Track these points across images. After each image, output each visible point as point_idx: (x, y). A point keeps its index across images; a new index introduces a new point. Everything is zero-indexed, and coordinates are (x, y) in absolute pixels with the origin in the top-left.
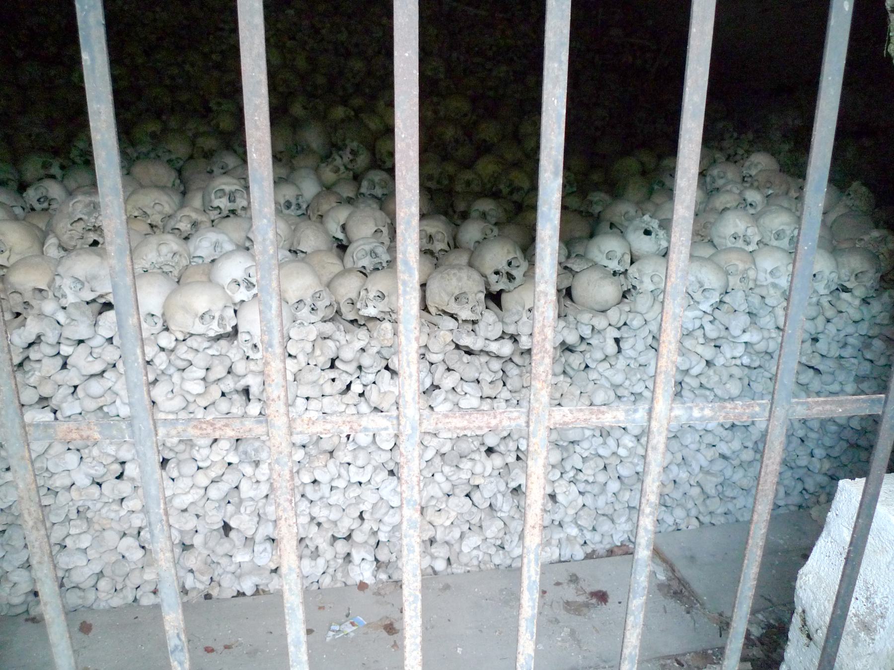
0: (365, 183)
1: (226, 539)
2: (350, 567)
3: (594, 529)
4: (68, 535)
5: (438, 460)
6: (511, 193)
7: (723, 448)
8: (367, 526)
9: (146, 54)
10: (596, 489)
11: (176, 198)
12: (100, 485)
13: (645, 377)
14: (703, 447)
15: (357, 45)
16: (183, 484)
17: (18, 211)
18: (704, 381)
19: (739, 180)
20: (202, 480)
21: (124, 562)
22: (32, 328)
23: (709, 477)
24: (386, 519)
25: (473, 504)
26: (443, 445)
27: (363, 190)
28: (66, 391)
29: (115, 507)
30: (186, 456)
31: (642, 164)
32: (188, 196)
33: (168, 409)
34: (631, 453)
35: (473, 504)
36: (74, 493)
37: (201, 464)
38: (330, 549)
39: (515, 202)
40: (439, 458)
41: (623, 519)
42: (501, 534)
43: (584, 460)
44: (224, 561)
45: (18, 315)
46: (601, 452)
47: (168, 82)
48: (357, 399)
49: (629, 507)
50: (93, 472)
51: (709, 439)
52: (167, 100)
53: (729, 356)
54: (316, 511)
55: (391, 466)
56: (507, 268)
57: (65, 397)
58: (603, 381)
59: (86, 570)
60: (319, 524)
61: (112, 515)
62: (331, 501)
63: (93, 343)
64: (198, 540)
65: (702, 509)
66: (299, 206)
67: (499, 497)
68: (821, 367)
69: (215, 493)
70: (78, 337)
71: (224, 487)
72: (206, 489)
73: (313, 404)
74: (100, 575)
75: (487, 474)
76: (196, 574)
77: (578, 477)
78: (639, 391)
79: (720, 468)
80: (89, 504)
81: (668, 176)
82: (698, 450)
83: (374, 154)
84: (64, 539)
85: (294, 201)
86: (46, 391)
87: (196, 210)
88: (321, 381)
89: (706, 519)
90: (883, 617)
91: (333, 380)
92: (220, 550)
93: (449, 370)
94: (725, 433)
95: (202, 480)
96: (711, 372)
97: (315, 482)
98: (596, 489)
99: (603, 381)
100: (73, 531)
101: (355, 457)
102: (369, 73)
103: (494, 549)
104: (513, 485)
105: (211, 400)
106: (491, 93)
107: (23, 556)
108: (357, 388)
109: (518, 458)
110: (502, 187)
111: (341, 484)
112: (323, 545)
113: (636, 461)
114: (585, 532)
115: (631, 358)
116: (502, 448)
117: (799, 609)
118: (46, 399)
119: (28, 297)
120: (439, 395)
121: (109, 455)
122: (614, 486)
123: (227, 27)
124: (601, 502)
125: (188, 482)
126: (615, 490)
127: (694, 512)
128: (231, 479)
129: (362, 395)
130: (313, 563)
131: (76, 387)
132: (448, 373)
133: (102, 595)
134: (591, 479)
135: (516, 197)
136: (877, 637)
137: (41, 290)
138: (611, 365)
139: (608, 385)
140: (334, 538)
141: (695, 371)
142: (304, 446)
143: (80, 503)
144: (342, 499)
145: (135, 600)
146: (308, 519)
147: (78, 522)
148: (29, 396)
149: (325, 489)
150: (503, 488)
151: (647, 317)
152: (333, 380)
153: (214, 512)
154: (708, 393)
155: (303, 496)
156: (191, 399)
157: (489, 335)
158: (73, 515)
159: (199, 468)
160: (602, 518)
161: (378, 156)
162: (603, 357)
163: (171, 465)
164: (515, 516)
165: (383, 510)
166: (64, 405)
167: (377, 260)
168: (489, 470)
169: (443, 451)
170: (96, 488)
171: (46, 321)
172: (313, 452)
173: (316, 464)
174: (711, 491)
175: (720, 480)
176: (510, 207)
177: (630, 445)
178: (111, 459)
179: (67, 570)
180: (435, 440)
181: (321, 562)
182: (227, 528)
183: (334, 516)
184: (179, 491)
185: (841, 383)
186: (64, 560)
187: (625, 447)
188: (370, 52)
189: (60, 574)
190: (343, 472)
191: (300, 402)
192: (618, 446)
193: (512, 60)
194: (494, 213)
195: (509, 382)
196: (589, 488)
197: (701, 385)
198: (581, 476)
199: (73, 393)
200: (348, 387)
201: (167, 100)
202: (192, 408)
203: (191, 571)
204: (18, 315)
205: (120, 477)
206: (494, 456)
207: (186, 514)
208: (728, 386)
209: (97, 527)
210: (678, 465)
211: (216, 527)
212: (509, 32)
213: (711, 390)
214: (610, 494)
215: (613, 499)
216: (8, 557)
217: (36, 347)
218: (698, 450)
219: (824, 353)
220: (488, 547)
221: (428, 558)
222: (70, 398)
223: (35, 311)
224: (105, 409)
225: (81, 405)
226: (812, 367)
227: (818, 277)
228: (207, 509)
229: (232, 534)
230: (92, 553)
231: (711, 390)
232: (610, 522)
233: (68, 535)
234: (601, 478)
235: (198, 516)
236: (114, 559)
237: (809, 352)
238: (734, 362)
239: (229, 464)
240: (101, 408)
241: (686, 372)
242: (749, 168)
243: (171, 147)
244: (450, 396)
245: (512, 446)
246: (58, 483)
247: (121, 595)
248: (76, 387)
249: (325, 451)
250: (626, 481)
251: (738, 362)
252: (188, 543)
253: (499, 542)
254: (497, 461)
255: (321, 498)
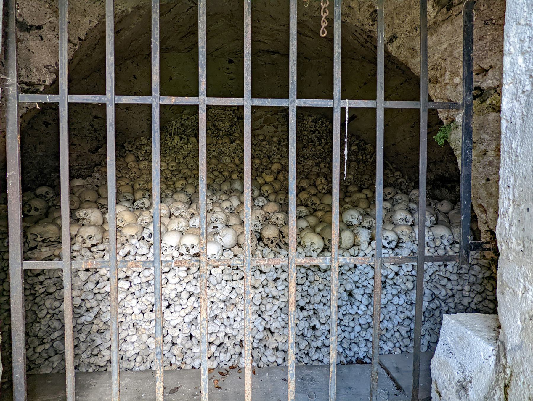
0: (256, 201)
1: (189, 341)
2: (241, 358)
3: (350, 350)
4: (128, 335)
5: (279, 311)
6: (312, 205)
7: (408, 313)
9: (184, 159)
10: (350, 329)
11: (187, 206)
12: (143, 313)
13: (368, 279)
14: (399, 312)
15: (257, 155)
16: (175, 315)
17: (131, 209)
18: (395, 281)
19: (408, 200)
20: (183, 313)
21: (148, 349)
22: (127, 248)
23: (403, 327)
24: (257, 336)
26: (281, 304)
27: (255, 204)
28: (136, 274)
29: (148, 324)
30: (177, 303)
31: (366, 195)
32: (192, 205)
34: (364, 313)
36: (133, 317)
37: (183, 307)
38: (233, 349)
39: (313, 209)
40: (279, 310)
41: (364, 345)
42: (307, 348)
43: (344, 315)
44: (188, 352)
45: (124, 244)
46: (351, 312)
47: (190, 168)
49: (366, 340)
50: (141, 308)
51: (400, 309)
52: (189, 173)
53: (405, 271)
54: (227, 330)
55: (259, 313)
57: (135, 276)
58: (350, 280)
59: (133, 351)
60: (229, 337)
61: (146, 327)
62: (234, 327)
63: (148, 256)
64: (179, 341)
65: (401, 344)
66: (231, 209)
67: (306, 330)
68: (451, 278)
69: (188, 319)
70: (142, 253)
71: (191, 317)
72: (184, 317)
73: (229, 284)
74: (138, 354)
75: (300, 319)
76: (177, 356)
77: (341, 323)
78: (366, 285)
79: (408, 324)
80: (138, 322)
82: (396, 314)
83: (261, 191)
84: (126, 337)
85: (229, 207)
86: (128, 274)
87: (194, 210)
88: (232, 274)
89: (404, 349)
90: (470, 382)
91: (237, 274)
92: (187, 346)
93: (283, 271)
94: (408, 306)
95: (183, 313)
96: (398, 277)
97: (228, 317)
98: (350, 329)
99: (350, 280)
100: (130, 333)
102: (261, 164)
103: (304, 355)
104: (312, 325)
105: (189, 280)
106: (306, 171)
107: (109, 344)
109: (315, 313)
110: (309, 202)
111: (238, 319)
112: (230, 348)
113: (367, 317)
114: (346, 350)
115: (361, 270)
116: (307, 307)
117: (434, 380)
118: (129, 277)
119: (128, 237)
120: (279, 282)
121: (148, 301)
122: (358, 328)
123: (212, 150)
124: (352, 336)
125: (177, 314)
126: (359, 331)
127: (397, 345)
128: (194, 313)
130: (225, 355)
131: (140, 273)
132: (282, 273)
133: (137, 364)
134: (347, 325)
135: (314, 207)
136: (470, 393)
137: (133, 236)
138: (353, 273)
139: (352, 282)
140: (235, 344)
141: (390, 277)
142: (224, 302)
143: (134, 321)
144: (239, 326)
145: (150, 368)
146: (224, 334)
147: (133, 329)
148: (122, 275)
149: (232, 321)
150: (307, 326)
151: (366, 252)
152: (237, 274)
153: (186, 328)
154: (398, 287)
155: (222, 323)
156: (182, 279)
158: (131, 326)
159: (182, 308)
160: (353, 344)
161: (262, 192)
162: (349, 269)
163: (171, 307)
165: (255, 332)
166: (135, 280)
167: (256, 228)
168: (301, 317)
169: (281, 307)
170: (142, 315)
171: (132, 246)
173: (229, 309)
174: (405, 335)
175: (409, 329)
176: (311, 210)
177: (364, 309)
178: (149, 303)
179: (126, 351)
180: (278, 302)
181: (228, 355)
182: (191, 336)
183: (235, 333)
184: (173, 318)
185: (462, 285)
186: (124, 347)
187: (361, 310)
188: (262, 157)
189: (122, 353)
190: (239, 313)
192: (358, 309)
193: (315, 159)
194: (304, 212)
195: (309, 278)
196: (346, 329)
197: (395, 284)
198: (342, 323)
199: (139, 275)
201: (189, 173)
202: (182, 282)
203: (175, 355)
204: (124, 244)
205: (152, 311)
206: (303, 311)
207: (175, 329)
208: (406, 284)
209: (140, 332)
210: (388, 321)
211: (186, 335)
212: (314, 149)
213: (399, 286)
214: (356, 333)
215: (358, 335)
216: (103, 344)
217: (128, 257)
218: (396, 314)
219: (451, 271)
220: (302, 354)
221: (275, 357)
222: (137, 277)
223: (129, 243)
224: (150, 282)
225: (141, 280)
226: (447, 278)
227: (444, 237)
228: (184, 327)
229: (193, 339)
230: (136, 344)
231: (399, 286)
232: (357, 347)
233: (128, 335)
234: (352, 324)
235: (180, 330)
236: (144, 347)
237: (444, 270)
238: (408, 273)
239: (194, 307)
240: (148, 282)
241: (386, 277)
242: (412, 195)
244: (285, 283)
245: (311, 307)
246: (127, 312)
247: (145, 365)
248: (140, 273)
249: (233, 304)
250: (363, 326)
251: (410, 273)
252: (175, 342)
253: (306, 352)
254: (305, 313)
255: (230, 325)
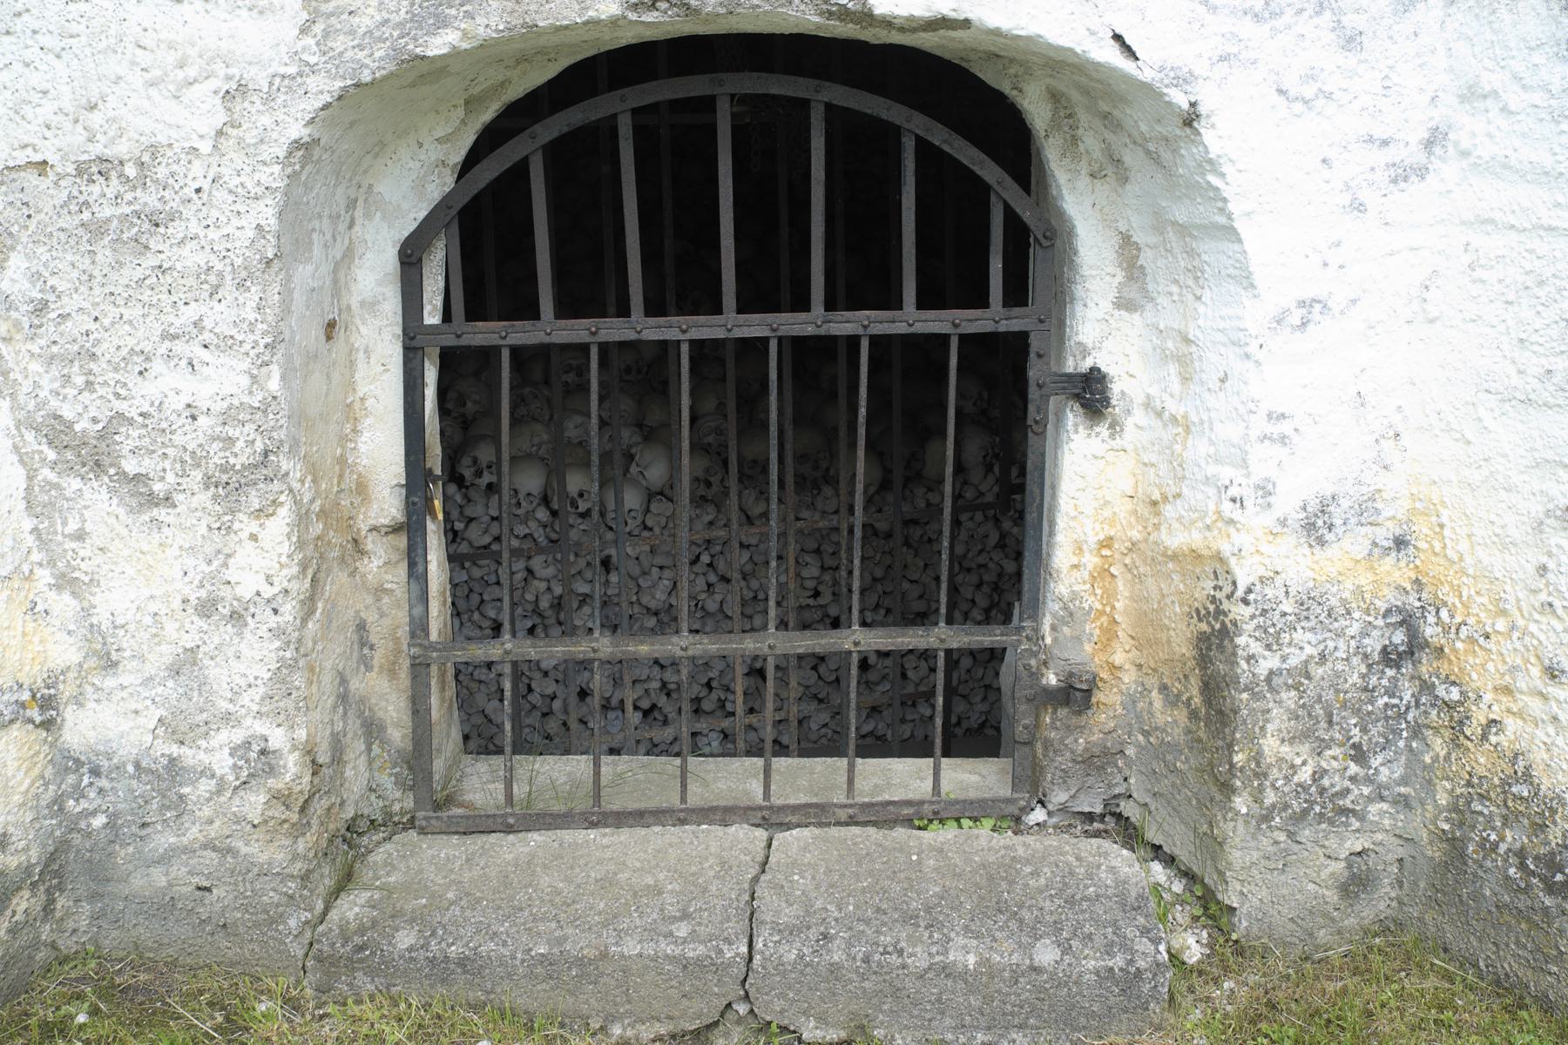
8: (714, 696)
25: (820, 677)
33: (544, 576)
35: (820, 677)
41: (979, 698)
48: (705, 569)
56: (484, 465)
81: (1073, 417)
101: (704, 625)
108: (705, 559)
129: (710, 565)
157: (826, 508)
164: (1011, 524)
172: (666, 619)
191: (655, 571)
200: (698, 557)
214: (963, 672)
243: (1081, 429)
